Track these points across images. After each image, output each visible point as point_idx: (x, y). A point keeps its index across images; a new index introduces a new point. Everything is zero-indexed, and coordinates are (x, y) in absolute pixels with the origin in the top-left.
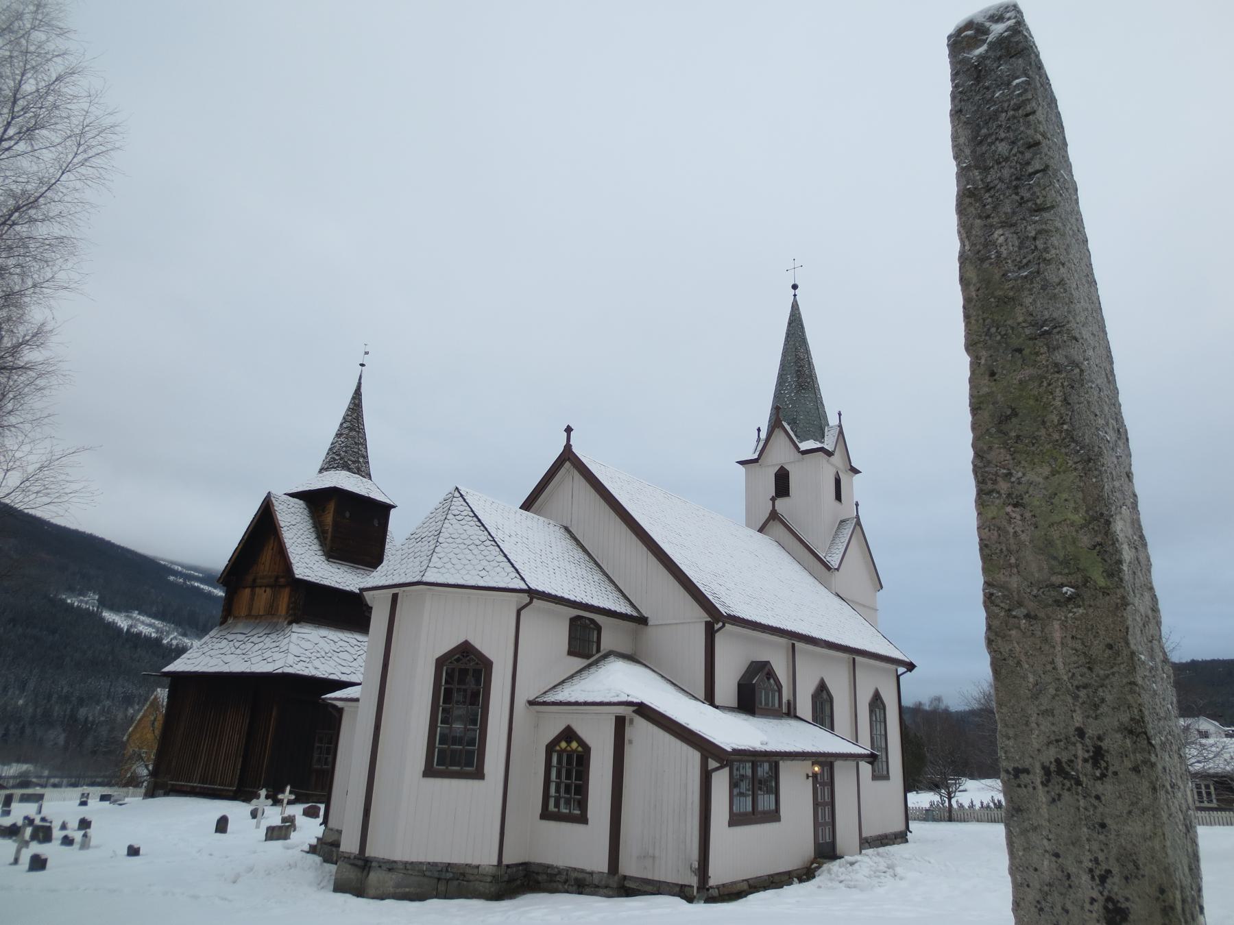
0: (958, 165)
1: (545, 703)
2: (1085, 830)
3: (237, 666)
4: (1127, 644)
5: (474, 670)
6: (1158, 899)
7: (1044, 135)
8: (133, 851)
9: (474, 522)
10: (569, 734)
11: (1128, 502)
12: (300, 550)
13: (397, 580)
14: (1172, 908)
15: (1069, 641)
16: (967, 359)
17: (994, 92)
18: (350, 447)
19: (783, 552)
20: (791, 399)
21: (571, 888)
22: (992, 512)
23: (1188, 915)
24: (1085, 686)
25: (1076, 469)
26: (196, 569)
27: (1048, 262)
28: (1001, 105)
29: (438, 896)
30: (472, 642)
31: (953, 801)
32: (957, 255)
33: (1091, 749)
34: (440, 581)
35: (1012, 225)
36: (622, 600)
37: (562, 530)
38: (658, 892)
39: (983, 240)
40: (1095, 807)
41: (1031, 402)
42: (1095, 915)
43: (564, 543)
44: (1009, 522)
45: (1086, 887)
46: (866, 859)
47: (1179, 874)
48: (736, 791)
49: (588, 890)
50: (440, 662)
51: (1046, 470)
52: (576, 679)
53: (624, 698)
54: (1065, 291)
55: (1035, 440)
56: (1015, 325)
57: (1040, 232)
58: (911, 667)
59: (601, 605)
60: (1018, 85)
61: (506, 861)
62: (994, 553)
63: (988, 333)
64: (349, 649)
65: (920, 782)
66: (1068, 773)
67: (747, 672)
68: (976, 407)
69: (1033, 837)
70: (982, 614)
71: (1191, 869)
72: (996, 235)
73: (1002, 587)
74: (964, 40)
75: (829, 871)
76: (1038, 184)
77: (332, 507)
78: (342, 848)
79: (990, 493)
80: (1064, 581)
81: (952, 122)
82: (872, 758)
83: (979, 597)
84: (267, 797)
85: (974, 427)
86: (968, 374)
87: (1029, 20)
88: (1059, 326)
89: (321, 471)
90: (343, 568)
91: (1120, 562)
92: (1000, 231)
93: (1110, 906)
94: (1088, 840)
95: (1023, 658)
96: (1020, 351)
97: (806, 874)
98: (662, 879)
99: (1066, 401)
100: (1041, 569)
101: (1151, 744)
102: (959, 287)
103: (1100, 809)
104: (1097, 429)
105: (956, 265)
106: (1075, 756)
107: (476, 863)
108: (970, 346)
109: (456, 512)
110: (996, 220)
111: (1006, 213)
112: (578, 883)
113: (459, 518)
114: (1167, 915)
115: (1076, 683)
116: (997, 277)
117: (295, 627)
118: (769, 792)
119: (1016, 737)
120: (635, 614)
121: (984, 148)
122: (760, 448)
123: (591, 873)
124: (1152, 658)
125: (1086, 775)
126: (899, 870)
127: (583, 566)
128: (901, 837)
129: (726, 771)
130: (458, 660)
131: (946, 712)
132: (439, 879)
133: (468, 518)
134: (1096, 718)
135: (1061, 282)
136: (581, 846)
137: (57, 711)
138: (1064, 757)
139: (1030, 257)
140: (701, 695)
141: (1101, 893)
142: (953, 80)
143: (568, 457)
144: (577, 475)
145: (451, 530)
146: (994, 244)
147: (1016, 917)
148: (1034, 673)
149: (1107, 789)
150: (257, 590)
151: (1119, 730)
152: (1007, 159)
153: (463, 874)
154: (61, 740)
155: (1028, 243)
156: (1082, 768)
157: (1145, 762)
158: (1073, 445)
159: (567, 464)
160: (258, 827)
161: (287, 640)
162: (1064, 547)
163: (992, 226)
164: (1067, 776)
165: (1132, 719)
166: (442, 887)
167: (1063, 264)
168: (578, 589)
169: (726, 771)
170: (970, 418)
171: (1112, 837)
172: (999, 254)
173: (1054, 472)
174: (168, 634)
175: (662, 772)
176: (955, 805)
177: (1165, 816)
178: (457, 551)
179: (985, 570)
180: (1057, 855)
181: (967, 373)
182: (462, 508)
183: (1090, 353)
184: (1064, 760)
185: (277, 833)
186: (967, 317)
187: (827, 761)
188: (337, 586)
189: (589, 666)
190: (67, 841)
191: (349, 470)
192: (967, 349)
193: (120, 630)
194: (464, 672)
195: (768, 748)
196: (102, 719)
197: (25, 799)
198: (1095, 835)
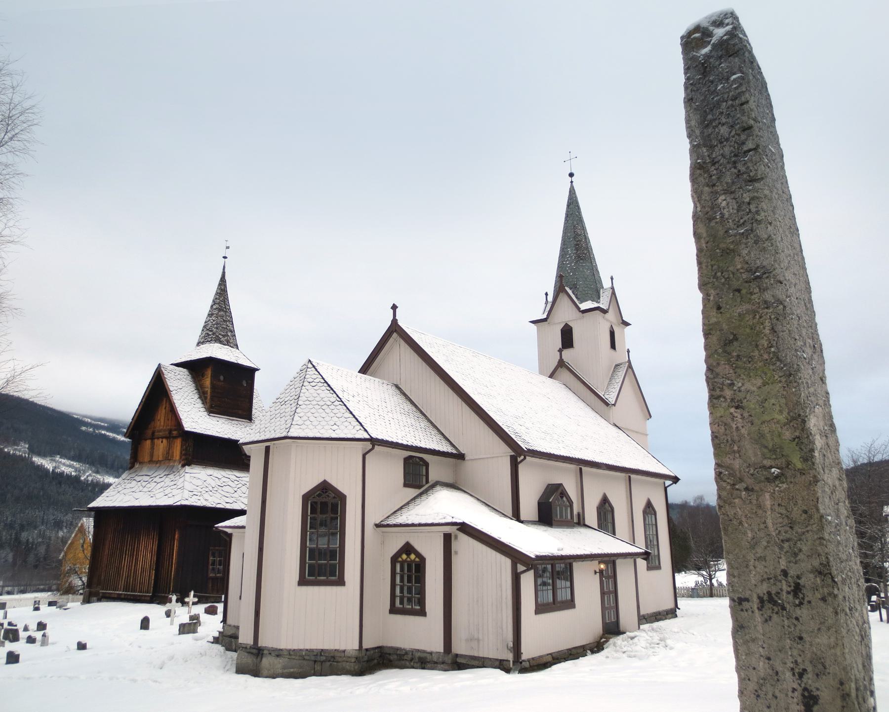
0: (691, 143)
1: (388, 526)
2: (788, 641)
4: (818, 510)
6: (839, 688)
7: (755, 120)
8: (82, 646)
10: (408, 548)
12: (187, 408)
14: (848, 695)
15: (776, 507)
16: (699, 296)
17: (717, 86)
19: (571, 394)
21: (415, 665)
22: (720, 412)
23: (861, 699)
25: (780, 382)
27: (759, 222)
28: (723, 86)
29: (315, 675)
30: (329, 481)
31: (714, 581)
33: (793, 584)
34: (302, 435)
35: (732, 193)
36: (444, 442)
37: (394, 388)
38: (483, 666)
39: (710, 204)
41: (748, 330)
42: (795, 700)
43: (395, 398)
44: (733, 420)
45: (789, 680)
46: (643, 634)
47: (855, 671)
48: (540, 581)
49: (429, 665)
50: (306, 498)
51: (759, 382)
52: (411, 506)
53: (449, 520)
55: (751, 359)
56: (735, 271)
57: (752, 199)
58: (675, 480)
59: (428, 447)
61: (365, 646)
62: (723, 443)
64: (230, 483)
66: (776, 602)
67: (544, 493)
68: (708, 332)
69: (753, 646)
71: (864, 666)
72: (720, 200)
73: (728, 468)
74: (693, 40)
75: (614, 644)
77: (209, 373)
79: (718, 398)
80: (773, 464)
81: (686, 107)
82: (646, 556)
84: (177, 601)
86: (701, 307)
87: (744, 23)
88: (767, 272)
89: (198, 344)
91: (812, 450)
92: (723, 197)
93: (806, 694)
94: (790, 648)
95: (744, 519)
97: (597, 647)
98: (485, 656)
99: (773, 330)
100: (756, 455)
101: (834, 581)
102: (693, 240)
103: (799, 627)
104: (796, 350)
105: (691, 222)
106: (781, 590)
107: (342, 648)
108: (702, 286)
111: (727, 183)
113: (313, 384)
114: (845, 699)
115: (781, 538)
116: (721, 233)
117: (187, 469)
119: (739, 576)
120: (454, 452)
121: (710, 130)
123: (431, 653)
124: (838, 516)
125: (789, 603)
126: (669, 642)
127: (411, 416)
128: (672, 613)
129: (531, 573)
130: (319, 495)
131: (708, 507)
132: (315, 661)
134: (796, 563)
135: (769, 238)
136: (422, 633)
139: (746, 218)
140: (510, 514)
141: (800, 685)
142: (685, 73)
143: (395, 329)
144: (403, 343)
145: (307, 394)
146: (719, 206)
147: (741, 701)
148: (752, 530)
149: (803, 613)
152: (727, 140)
153: (334, 657)
154: (10, 557)
155: (744, 207)
156: (786, 598)
157: (830, 594)
158: (778, 363)
159: (395, 335)
160: (172, 624)
161: (182, 479)
162: (773, 439)
163: (717, 193)
164: (775, 603)
165: (821, 564)
167: (770, 224)
168: (409, 435)
169: (531, 573)
170: (703, 340)
171: (807, 646)
172: (722, 215)
174: (84, 472)
175: (482, 581)
176: (715, 584)
177: (844, 631)
178: (313, 411)
179: (716, 455)
180: (769, 659)
181: (700, 307)
184: (773, 592)
186: (700, 263)
187: (610, 560)
189: (421, 495)
190: (31, 640)
191: (221, 342)
192: (700, 288)
193: (47, 471)
194: (324, 505)
195: (564, 553)
196: (40, 540)
198: (795, 645)
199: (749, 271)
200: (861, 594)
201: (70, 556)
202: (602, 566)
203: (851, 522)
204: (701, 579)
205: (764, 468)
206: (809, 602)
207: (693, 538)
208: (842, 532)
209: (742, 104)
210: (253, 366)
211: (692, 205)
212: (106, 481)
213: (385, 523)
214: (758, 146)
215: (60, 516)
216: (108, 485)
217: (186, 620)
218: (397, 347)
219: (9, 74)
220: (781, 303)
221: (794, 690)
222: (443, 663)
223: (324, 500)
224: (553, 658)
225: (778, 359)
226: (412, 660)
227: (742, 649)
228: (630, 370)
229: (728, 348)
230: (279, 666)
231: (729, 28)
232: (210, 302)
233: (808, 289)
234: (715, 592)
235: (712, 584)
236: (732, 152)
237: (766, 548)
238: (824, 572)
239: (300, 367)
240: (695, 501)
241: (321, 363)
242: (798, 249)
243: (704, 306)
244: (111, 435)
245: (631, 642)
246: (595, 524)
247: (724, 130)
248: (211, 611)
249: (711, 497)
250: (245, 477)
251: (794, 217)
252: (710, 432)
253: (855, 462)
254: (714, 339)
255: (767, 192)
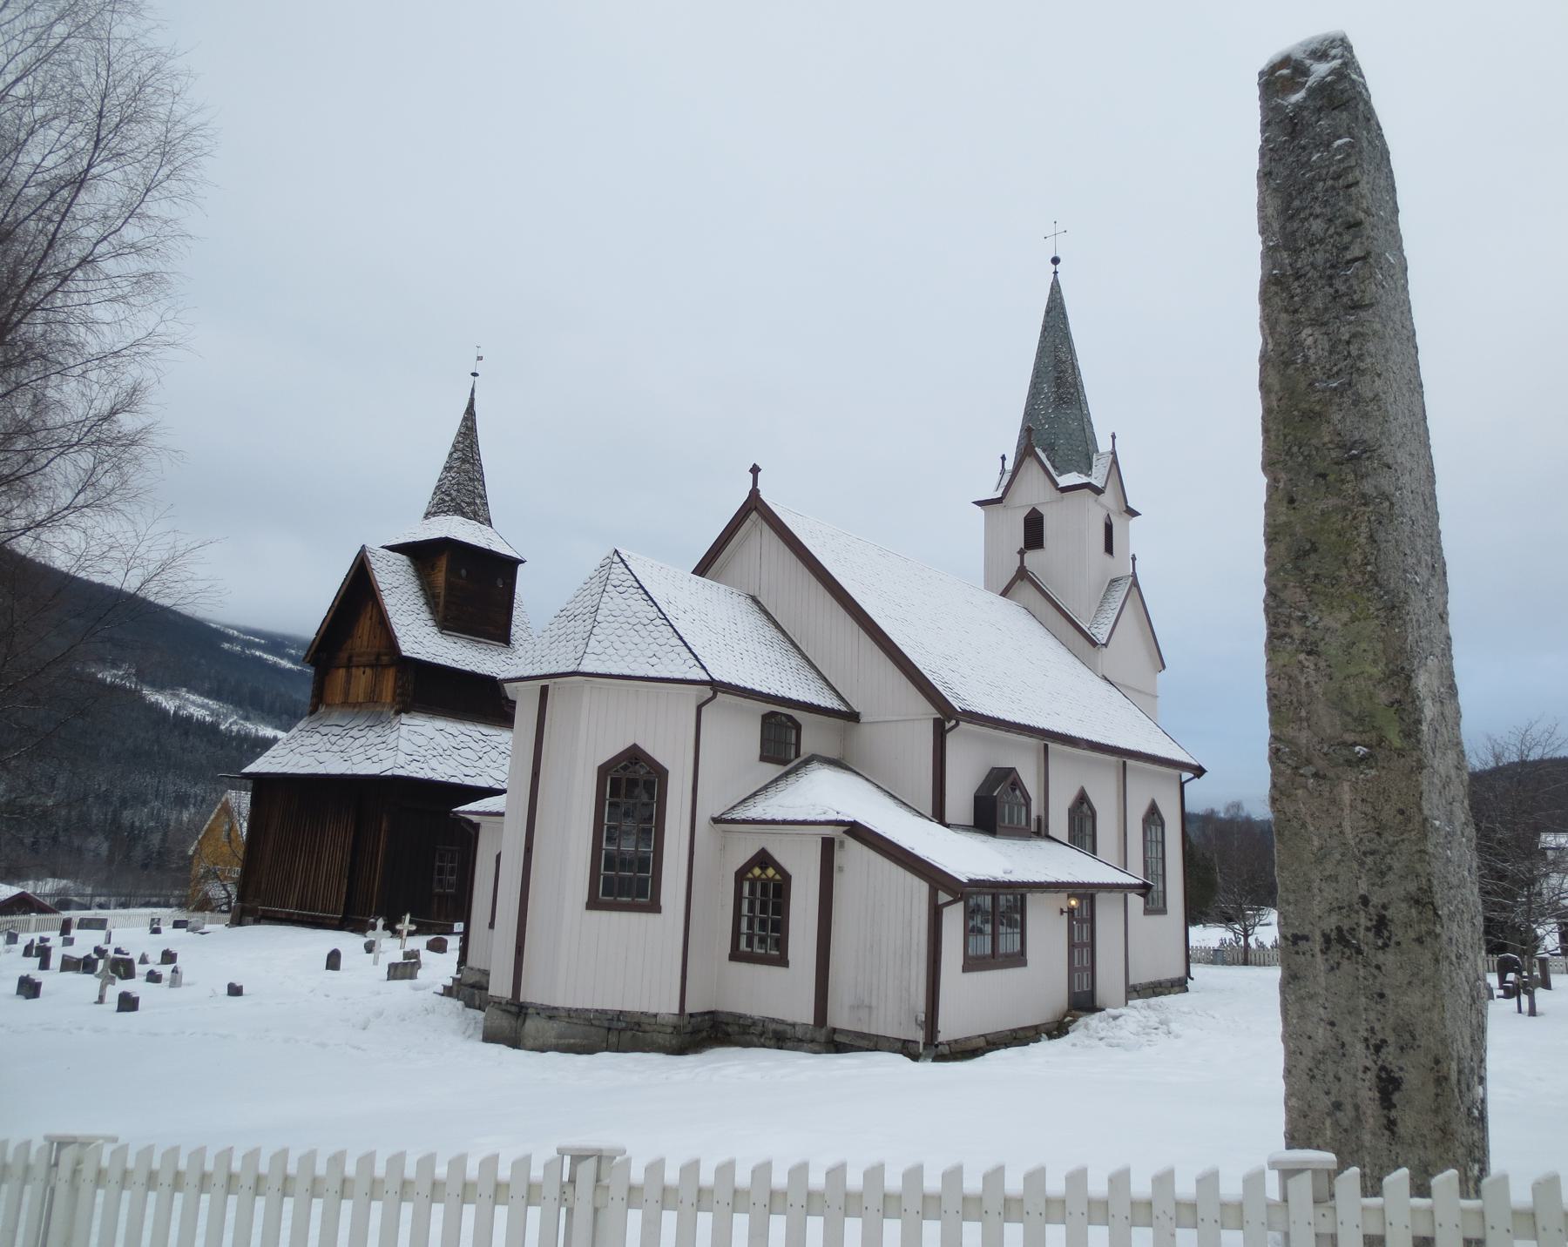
0: (1264, 242)
1: (733, 821)
3: (334, 766)
4: (1420, 810)
7: (1367, 212)
8: (234, 991)
9: (640, 595)
10: (763, 859)
11: (1437, 651)
12: (406, 620)
13: (546, 670)
14: (1446, 1079)
16: (1263, 481)
18: (463, 485)
22: (1283, 658)
23: (1464, 1086)
24: (1373, 853)
26: (256, 633)
27: (1362, 372)
28: (1318, 134)
29: (607, 1049)
31: (1251, 940)
35: (1323, 324)
36: (827, 691)
37: (749, 601)
40: (1375, 977)
41: (1333, 537)
42: (1367, 1084)
43: (751, 618)
44: (1302, 671)
45: (1360, 1055)
49: (789, 1044)
50: (603, 770)
52: (771, 791)
53: (832, 816)
54: (1380, 408)
55: (1335, 581)
57: (1354, 336)
58: (1199, 771)
59: (801, 699)
60: (1339, 147)
61: (689, 1009)
62: (1284, 704)
63: (1289, 452)
64: (472, 744)
68: (1272, 536)
69: (1309, 1005)
70: (1267, 770)
71: (1473, 1041)
72: (1303, 335)
73: (1290, 742)
74: (1279, 79)
75: (1086, 1026)
76: (1357, 276)
77: (443, 563)
78: (491, 992)
80: (1358, 739)
81: (1259, 186)
82: (1144, 889)
83: (1265, 751)
84: (385, 928)
85: (1269, 560)
87: (1362, 55)
88: (1369, 450)
89: (427, 516)
90: (461, 643)
91: (1419, 722)
92: (1308, 331)
93: (1384, 1075)
95: (1309, 820)
96: (1324, 476)
97: (1058, 1029)
99: (1372, 539)
103: (1380, 979)
104: (1405, 571)
107: (653, 1010)
108: (1269, 465)
112: (779, 1037)
113: (621, 589)
115: (1363, 849)
116: (1303, 385)
117: (404, 718)
118: (1011, 924)
120: (843, 708)
123: (794, 1025)
124: (1450, 822)
126: (1174, 1026)
127: (776, 647)
128: (1180, 985)
129: (960, 906)
130: (625, 768)
131: (1248, 821)
134: (1382, 886)
135: (1376, 398)
136: (781, 992)
137: (96, 814)
139: (1342, 365)
142: (1263, 132)
143: (754, 505)
144: (766, 527)
145: (611, 605)
146: (1301, 345)
148: (1320, 836)
149: (1389, 959)
152: (1321, 241)
153: (639, 1024)
156: (1364, 937)
157: (1429, 933)
158: (1376, 589)
159: (754, 515)
160: (375, 963)
161: (394, 735)
163: (1299, 323)
164: (1347, 944)
166: (613, 1038)
167: (1379, 375)
169: (960, 906)
170: (1263, 549)
171: (1391, 1006)
172: (1306, 359)
173: (1354, 619)
174: (226, 717)
175: (883, 913)
176: (1253, 945)
177: (1446, 988)
178: (619, 632)
179: (1273, 723)
180: (1332, 1024)
182: (623, 577)
184: (1345, 928)
185: (404, 970)
186: (1266, 431)
187: (1087, 893)
188: (454, 665)
189: (786, 775)
190: (153, 977)
191: (464, 514)
192: (1264, 469)
193: (165, 712)
194: (633, 783)
195: (1013, 878)
197: (85, 924)
199: (1342, 446)
200: (1476, 936)
201: (208, 850)
202: (1073, 903)
203: (1471, 831)
204: (1229, 935)
205: (1344, 744)
206: (1398, 944)
207: (1222, 870)
208: (1455, 844)
209: (1349, 186)
210: (514, 555)
211: (1260, 340)
213: (728, 817)
214: (1369, 253)
215: (185, 787)
218: (757, 537)
219: (174, 76)
220: (1386, 497)
221: (1366, 1069)
222: (812, 1041)
223: (631, 776)
225: (1377, 583)
226: (761, 1035)
228: (1134, 589)
229: (1300, 563)
230: (553, 1033)
231: (1336, 63)
234: (1251, 957)
235: (1247, 945)
236: (1327, 261)
237: (1339, 863)
238: (1423, 901)
239: (599, 561)
240: (1228, 810)
243: (1269, 497)
244: (270, 658)
245: (1113, 1023)
246: (1065, 838)
248: (438, 947)
250: (501, 738)
251: (1417, 365)
252: (1265, 688)
253: (1497, 757)
254: (1281, 547)
255: (1377, 326)
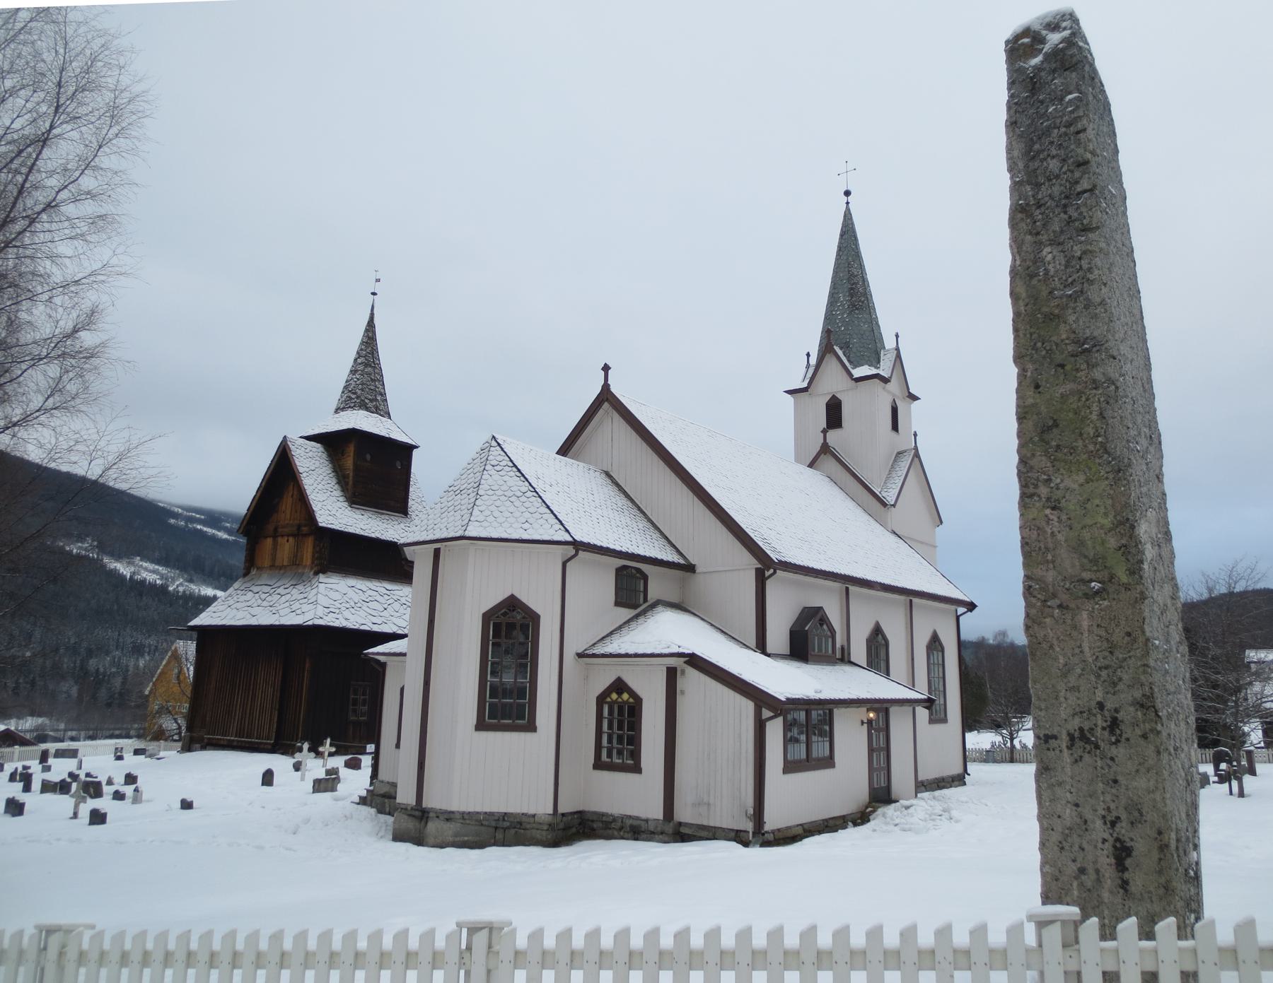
0: (1012, 178)
1: (594, 656)
4: (1143, 632)
5: (522, 626)
7: (1093, 153)
8: (186, 805)
9: (514, 472)
10: (619, 686)
12: (321, 497)
13: (438, 536)
14: (1167, 846)
16: (1014, 371)
18: (366, 385)
19: (836, 490)
20: (843, 320)
22: (1033, 513)
24: (1106, 667)
27: (1091, 282)
28: (1054, 95)
29: (494, 845)
31: (1016, 742)
32: (1008, 269)
36: (668, 548)
37: (603, 475)
41: (1071, 415)
44: (1048, 523)
45: (1099, 830)
46: (922, 803)
49: (644, 836)
50: (487, 617)
51: (1081, 478)
52: (624, 630)
53: (675, 650)
54: (1106, 311)
55: (1073, 450)
57: (1084, 252)
58: (971, 606)
59: (648, 554)
61: (561, 810)
62: (1035, 550)
64: (378, 598)
65: (980, 722)
67: (798, 619)
68: (1022, 417)
69: (1058, 791)
70: (1022, 603)
71: (1188, 815)
72: (1044, 253)
73: (1038, 580)
74: (1021, 46)
75: (884, 815)
76: (1085, 204)
77: (351, 449)
78: (398, 800)
79: (1031, 496)
81: (1007, 133)
82: (929, 703)
83: (1020, 588)
84: (310, 750)
85: (1020, 434)
86: (1015, 385)
88: (1097, 344)
89: (337, 411)
90: (367, 514)
91: (1141, 562)
92: (1048, 249)
93: (1118, 845)
95: (1055, 643)
96: (1062, 366)
97: (861, 818)
99: (1101, 416)
100: (1073, 566)
103: (1114, 768)
104: (1128, 441)
107: (532, 812)
108: (1019, 358)
109: (494, 463)
110: (1045, 237)
112: (635, 830)
113: (498, 468)
116: (1044, 294)
117: (322, 577)
119: (1047, 709)
120: (682, 561)
121: (1037, 164)
122: (809, 375)
123: (647, 821)
126: (954, 813)
127: (626, 513)
129: (780, 719)
130: (505, 614)
131: (1012, 646)
132: (496, 828)
133: (507, 469)
135: (1103, 303)
136: (637, 794)
137: (67, 663)
138: (1086, 726)
139: (1075, 276)
140: (753, 643)
142: (1009, 89)
143: (606, 397)
145: (490, 481)
146: (1043, 260)
148: (1064, 655)
149: (1120, 752)
150: (280, 539)
151: (1132, 704)
152: (1057, 177)
153: (521, 823)
154: (74, 691)
156: (1101, 735)
157: (1152, 730)
159: (606, 405)
160: (303, 779)
161: (314, 591)
163: (1041, 243)
164: (1088, 741)
165: (1144, 695)
166: (499, 835)
167: (1105, 284)
169: (780, 719)
171: (1122, 790)
172: (1047, 272)
174: (173, 580)
176: (1018, 746)
177: (1166, 773)
178: (498, 503)
179: (1026, 565)
180: (1077, 805)
181: (1013, 384)
182: (500, 458)
183: (1128, 367)
185: (327, 784)
186: (1016, 330)
187: (882, 707)
188: (362, 533)
189: (637, 617)
190: (118, 796)
191: (367, 409)
192: (1015, 361)
193: (122, 577)
194: (511, 626)
196: (114, 670)
197: (60, 754)
202: (871, 715)
204: (998, 739)
206: (1128, 739)
207: (990, 687)
208: (1171, 659)
209: (1078, 133)
211: (1010, 257)
212: (203, 593)
216: (215, 598)
217: (321, 774)
218: (609, 423)
221: (1104, 841)
223: (511, 620)
224: (805, 830)
225: (1106, 452)
227: (1045, 795)
228: (916, 460)
231: (1067, 33)
232: (353, 355)
233: (1148, 366)
234: (1016, 756)
235: (1013, 746)
238: (1147, 705)
240: (996, 637)
241: (509, 440)
242: (1138, 317)
243: (1020, 384)
247: (1053, 165)
248: (354, 765)
249: (1019, 637)
250: (402, 592)
253: (1210, 590)
254: (1030, 424)
255: (1103, 245)
